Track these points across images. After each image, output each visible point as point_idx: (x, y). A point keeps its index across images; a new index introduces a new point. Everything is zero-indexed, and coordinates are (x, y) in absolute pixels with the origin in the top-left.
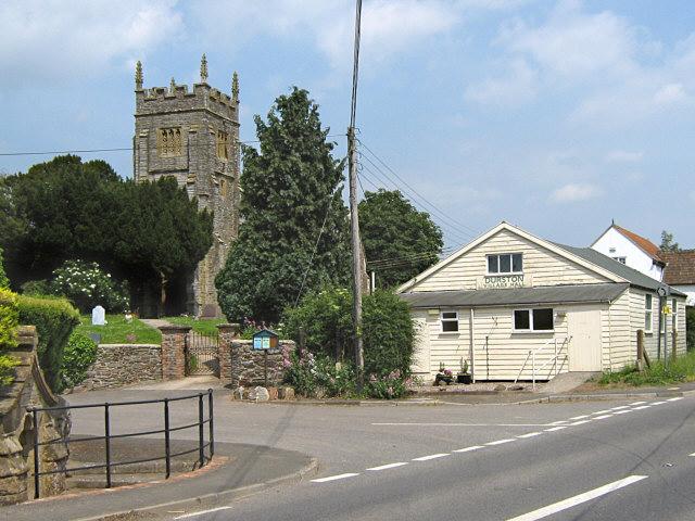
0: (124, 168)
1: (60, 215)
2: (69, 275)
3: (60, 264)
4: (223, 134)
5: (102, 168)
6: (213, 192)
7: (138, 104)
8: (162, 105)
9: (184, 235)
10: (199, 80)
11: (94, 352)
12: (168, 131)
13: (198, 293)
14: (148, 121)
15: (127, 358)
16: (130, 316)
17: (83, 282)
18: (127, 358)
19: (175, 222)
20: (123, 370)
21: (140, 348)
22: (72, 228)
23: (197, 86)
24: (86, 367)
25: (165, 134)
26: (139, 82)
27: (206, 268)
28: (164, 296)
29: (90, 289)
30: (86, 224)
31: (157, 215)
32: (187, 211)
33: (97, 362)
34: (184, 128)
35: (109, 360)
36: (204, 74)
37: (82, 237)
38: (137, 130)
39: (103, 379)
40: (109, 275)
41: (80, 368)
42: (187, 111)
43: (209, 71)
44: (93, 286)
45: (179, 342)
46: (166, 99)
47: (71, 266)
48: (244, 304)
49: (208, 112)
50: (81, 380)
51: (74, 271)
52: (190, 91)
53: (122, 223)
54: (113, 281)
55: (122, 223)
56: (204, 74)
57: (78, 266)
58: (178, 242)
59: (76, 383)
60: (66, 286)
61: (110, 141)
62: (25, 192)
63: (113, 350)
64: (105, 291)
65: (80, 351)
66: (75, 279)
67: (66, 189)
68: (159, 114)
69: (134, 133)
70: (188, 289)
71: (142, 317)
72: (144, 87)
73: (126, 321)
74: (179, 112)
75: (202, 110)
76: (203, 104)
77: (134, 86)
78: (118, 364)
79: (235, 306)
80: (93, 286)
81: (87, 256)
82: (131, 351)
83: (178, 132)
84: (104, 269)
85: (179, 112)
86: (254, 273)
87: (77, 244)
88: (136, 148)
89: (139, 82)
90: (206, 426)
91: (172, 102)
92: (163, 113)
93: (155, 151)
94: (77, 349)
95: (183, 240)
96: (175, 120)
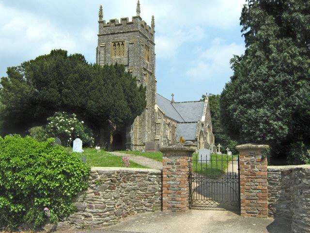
0: (91, 59)
1: (53, 83)
2: (57, 121)
3: (52, 115)
4: (148, 48)
5: (79, 58)
6: (142, 79)
7: (100, 29)
8: (117, 29)
9: (129, 99)
10: (135, 15)
11: (86, 176)
12: (117, 44)
13: (133, 138)
14: (105, 38)
15: (123, 184)
16: (99, 148)
17: (65, 126)
18: (123, 184)
19: (125, 91)
20: (119, 201)
21: (137, 172)
22: (60, 91)
23: (134, 18)
24: (74, 197)
25: (115, 45)
26: (101, 16)
27: (138, 123)
28: (112, 140)
29: (71, 130)
30: (69, 88)
31: (113, 85)
32: (132, 84)
33: (90, 190)
34: (126, 42)
35: (104, 189)
36: (138, 11)
37: (66, 97)
38: (99, 43)
39: (95, 214)
40: (83, 122)
41: (66, 197)
42: (128, 32)
43: (141, 10)
44: (72, 129)
45: (184, 167)
46: (116, 25)
47: (59, 116)
48: (278, 119)
49: (140, 33)
50: (67, 214)
51: (60, 119)
52: (130, 20)
53: (92, 88)
54: (84, 126)
55: (92, 88)
56: (138, 11)
57: (63, 116)
58: (126, 103)
59: (61, 218)
60: (55, 128)
61: (84, 44)
62: (32, 68)
63: (109, 175)
64: (80, 132)
65: (67, 175)
66: (61, 124)
67: (57, 67)
68: (112, 34)
69: (96, 45)
70: (127, 135)
71: (107, 150)
72: (103, 19)
73: (96, 151)
74: (124, 32)
75: (137, 31)
76: (137, 27)
77: (98, 19)
78: (114, 193)
79: (266, 122)
80: (72, 129)
81: (69, 109)
82: (128, 176)
83: (123, 44)
84: (79, 118)
85: (124, 32)
86: (284, 83)
87: (63, 102)
88: (98, 53)
89: (101, 16)
90: (94, 199)
91: (119, 27)
92: (114, 34)
93: (109, 55)
94: (64, 172)
95: (129, 102)
96: (121, 37)
